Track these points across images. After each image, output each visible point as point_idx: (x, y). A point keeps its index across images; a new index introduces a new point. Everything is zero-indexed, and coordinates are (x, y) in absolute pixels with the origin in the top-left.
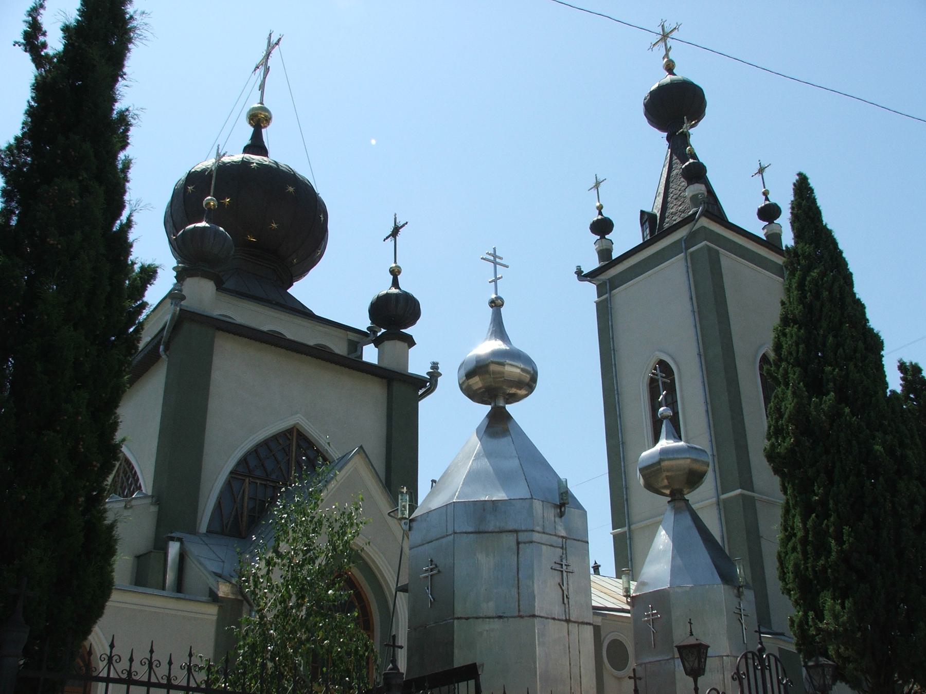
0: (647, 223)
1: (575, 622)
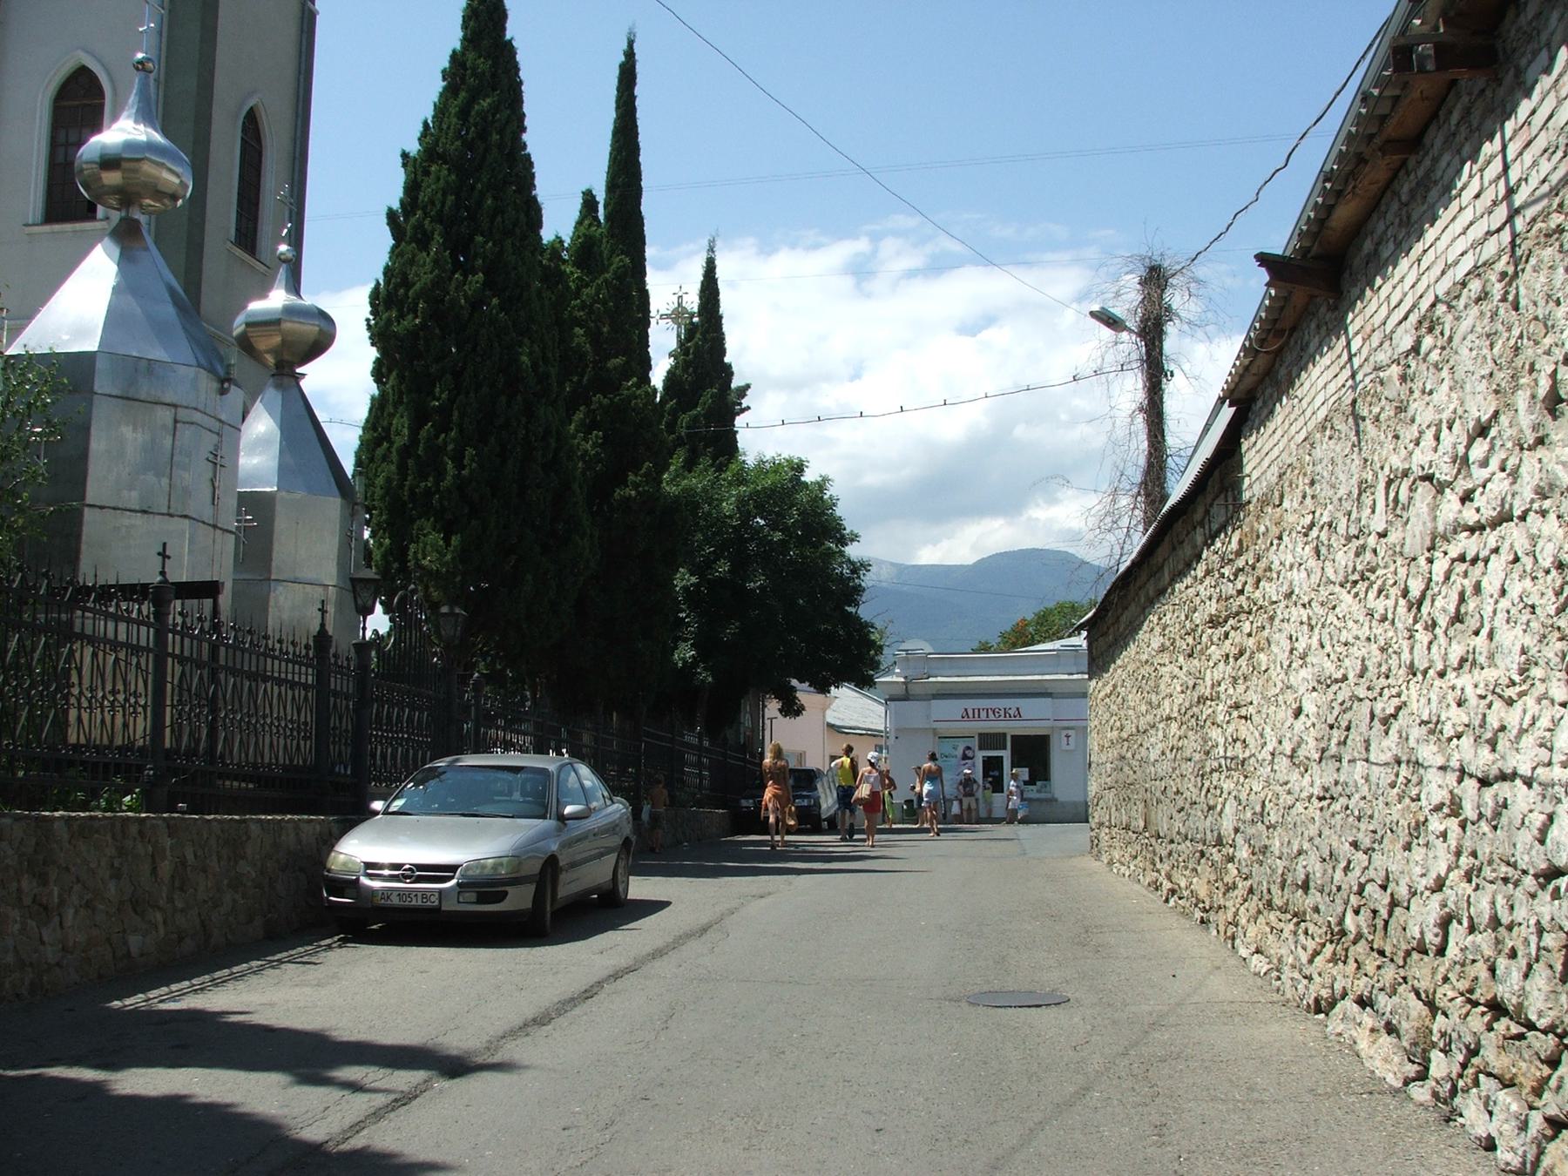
1: (221, 529)
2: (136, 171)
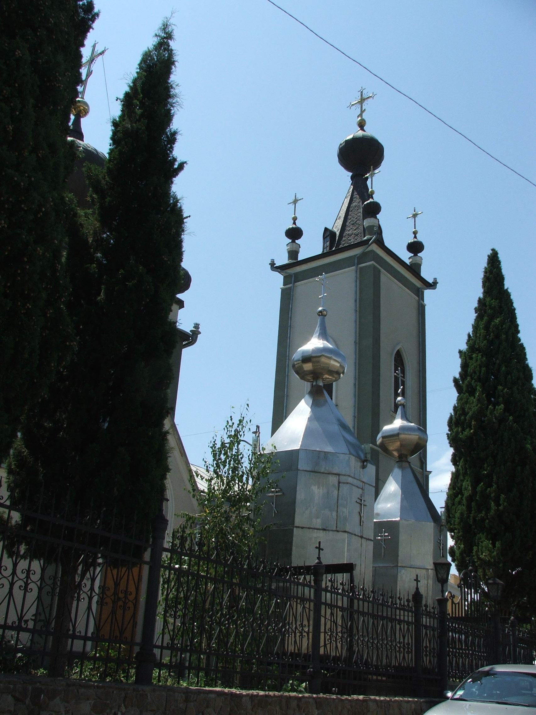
0: (328, 238)
1: (365, 538)
2: (318, 362)
